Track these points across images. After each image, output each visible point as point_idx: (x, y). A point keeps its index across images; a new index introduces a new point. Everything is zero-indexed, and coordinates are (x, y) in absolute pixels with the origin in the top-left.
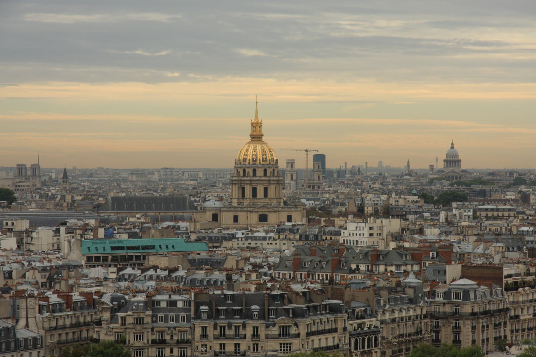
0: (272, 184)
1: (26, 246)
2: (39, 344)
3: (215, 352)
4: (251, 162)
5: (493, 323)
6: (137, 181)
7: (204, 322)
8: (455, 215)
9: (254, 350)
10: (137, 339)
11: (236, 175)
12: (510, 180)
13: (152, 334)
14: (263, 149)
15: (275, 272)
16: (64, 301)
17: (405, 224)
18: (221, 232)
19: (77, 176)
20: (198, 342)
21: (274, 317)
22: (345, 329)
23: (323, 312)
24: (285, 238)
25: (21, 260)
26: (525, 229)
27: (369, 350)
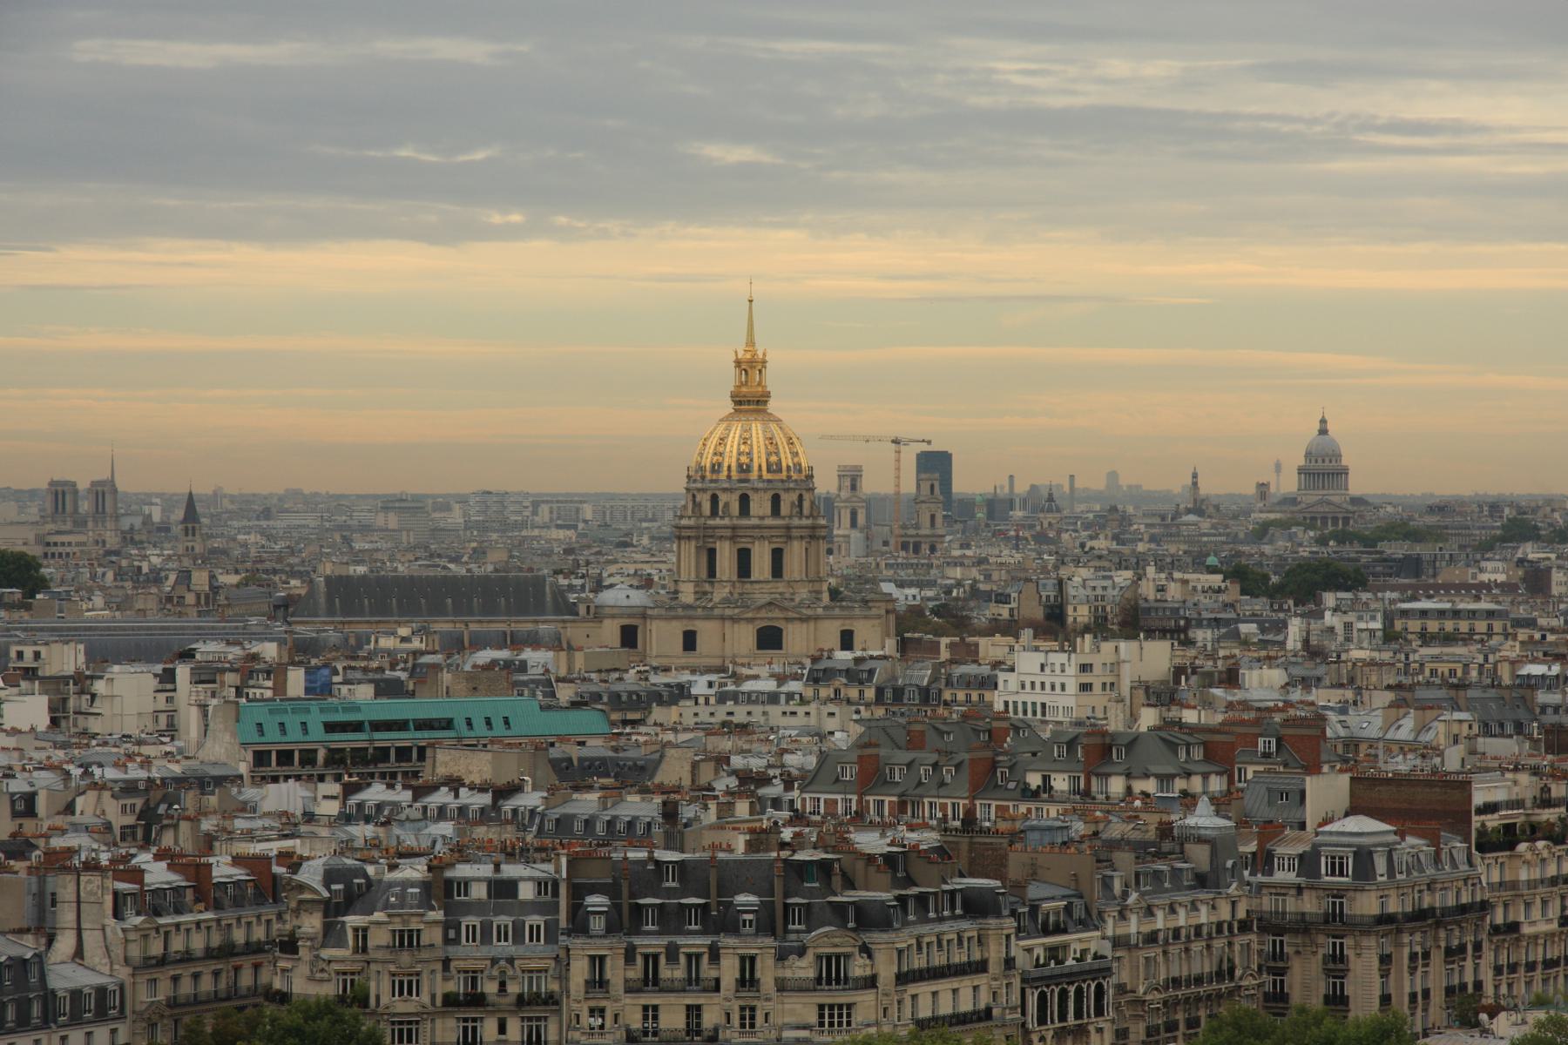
0: (796, 538)
1: (75, 720)
2: (114, 1008)
3: (628, 1031)
4: (734, 474)
5: (1443, 944)
6: (400, 530)
7: (598, 941)
8: (1331, 629)
9: (743, 1026)
10: (401, 994)
11: (690, 512)
12: (1493, 528)
13: (445, 979)
14: (769, 435)
15: (804, 795)
16: (188, 880)
18: (647, 679)
19: (225, 516)
20: (579, 1002)
21: (803, 927)
22: (1009, 963)
23: (946, 913)
24: (832, 696)
25: (61, 762)
26: (1537, 669)
27: (1080, 1025)
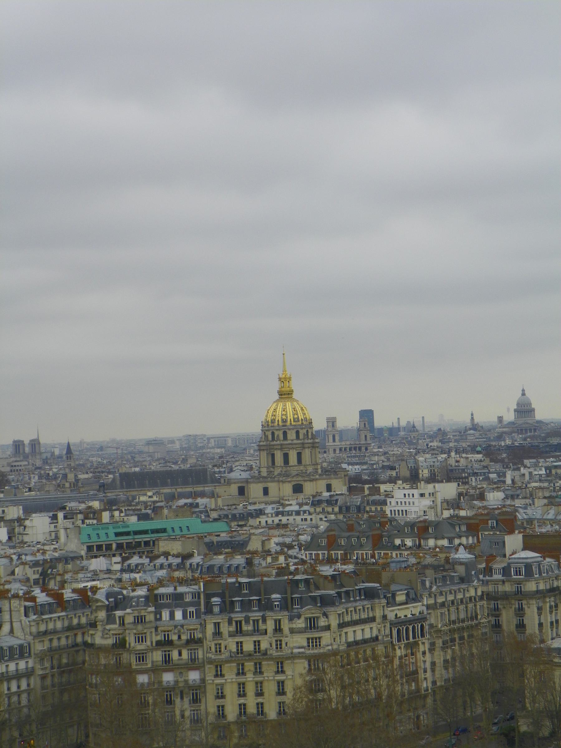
1: (18, 537)
2: (27, 653)
4: (280, 423)
6: (154, 452)
8: (524, 475)
9: (277, 648)
10: (139, 642)
11: (263, 440)
13: (156, 635)
16: (54, 600)
17: (464, 488)
18: (246, 508)
19: (85, 450)
20: (211, 642)
24: (321, 511)
25: (10, 555)
27: (415, 642)
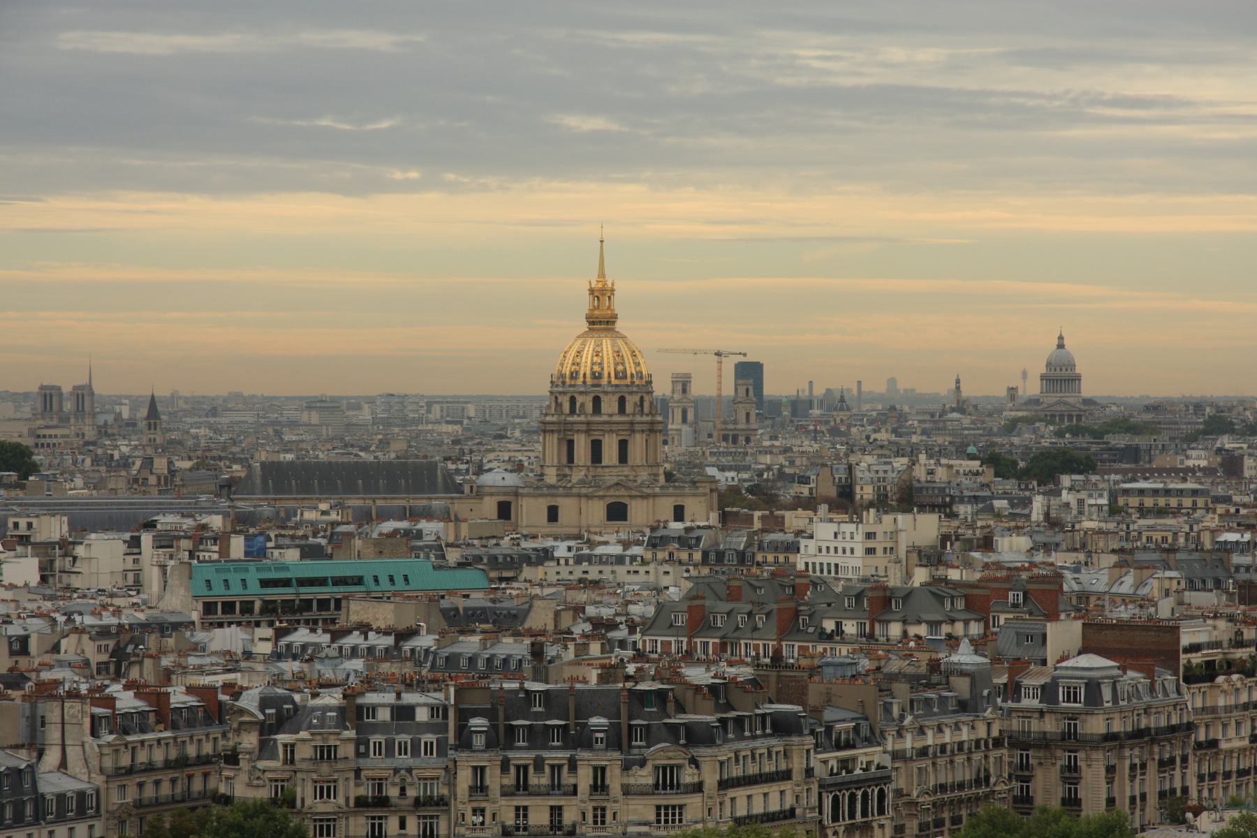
0: (638, 431)
1: (60, 577)
2: (92, 808)
3: (504, 827)
4: (588, 380)
5: (1157, 757)
6: (320, 425)
7: (480, 755)
8: (1067, 505)
9: (595, 822)
10: (321, 797)
11: (553, 411)
12: (1197, 423)
13: (357, 785)
14: (616, 349)
15: (645, 638)
16: (150, 706)
17: (949, 526)
18: (518, 545)
19: (181, 414)
20: (464, 803)
21: (643, 743)
23: (758, 732)
24: (667, 558)
25: (49, 611)
26: (1232, 537)
27: (865, 822)
